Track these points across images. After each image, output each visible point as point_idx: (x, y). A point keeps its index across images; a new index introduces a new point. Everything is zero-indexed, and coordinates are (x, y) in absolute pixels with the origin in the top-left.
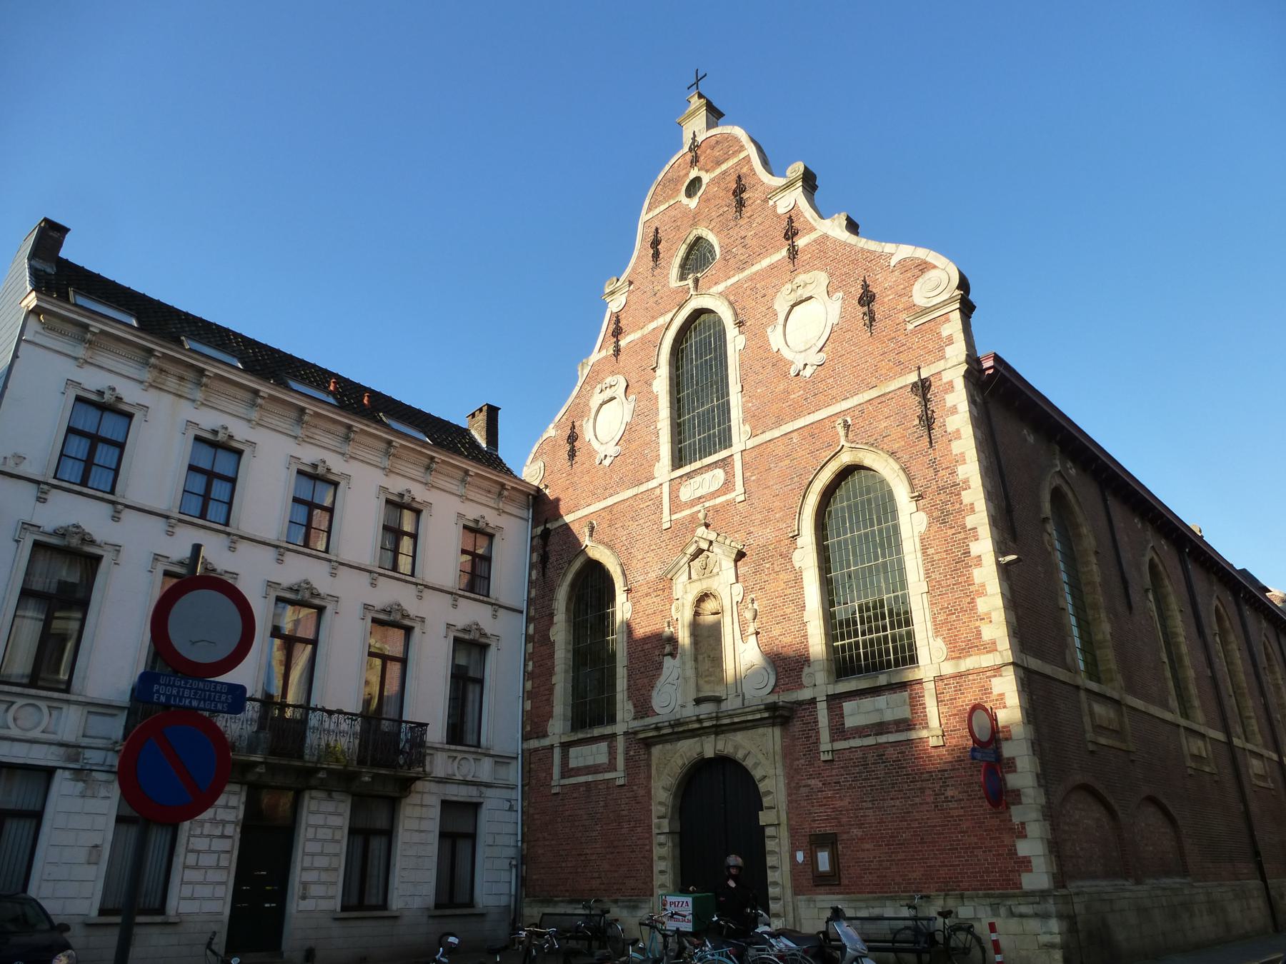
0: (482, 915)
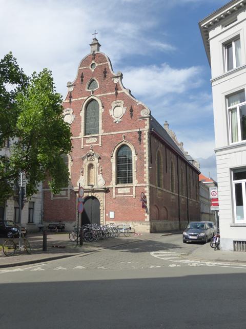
0: (35, 225)
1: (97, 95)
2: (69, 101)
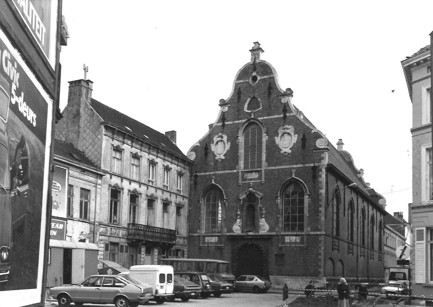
2: (221, 124)
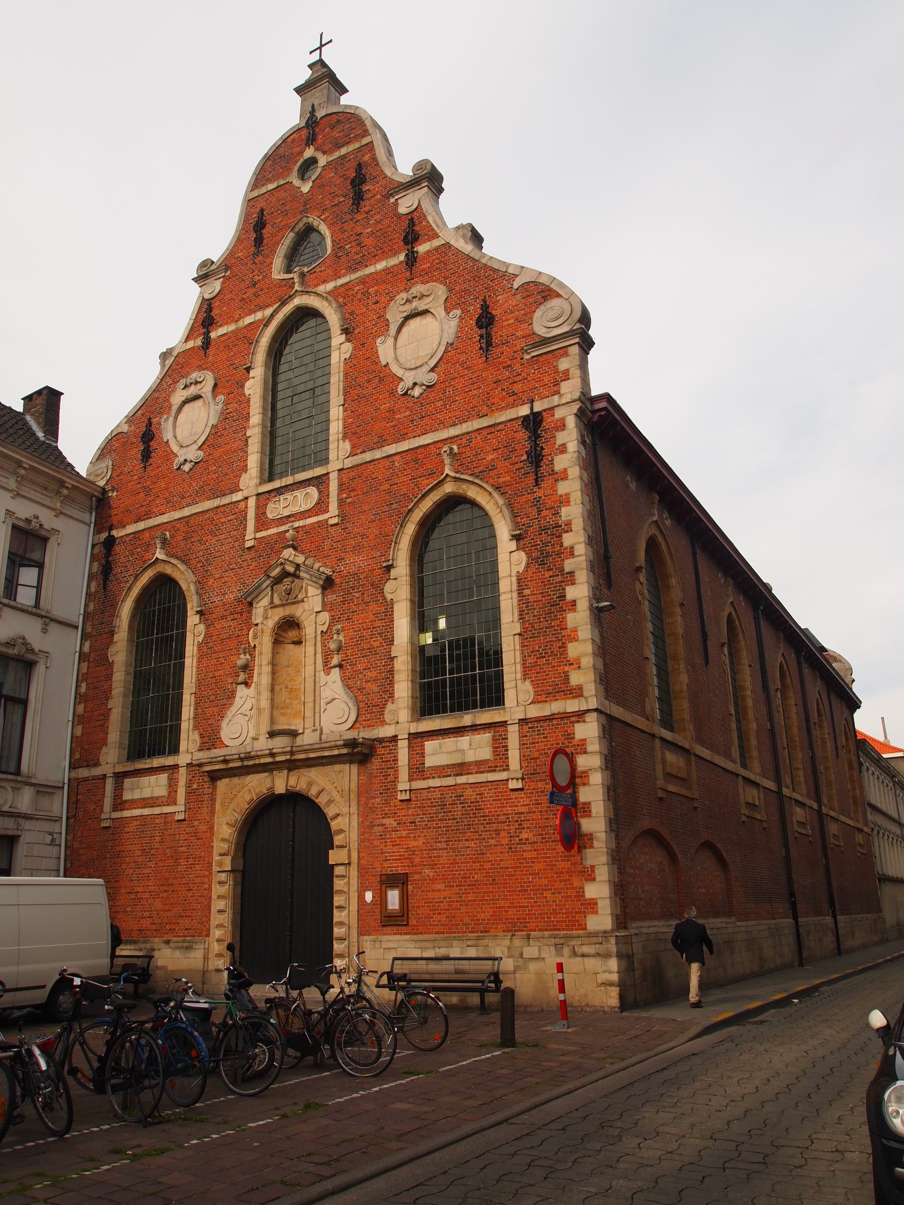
1: (321, 289)
2: (199, 342)
